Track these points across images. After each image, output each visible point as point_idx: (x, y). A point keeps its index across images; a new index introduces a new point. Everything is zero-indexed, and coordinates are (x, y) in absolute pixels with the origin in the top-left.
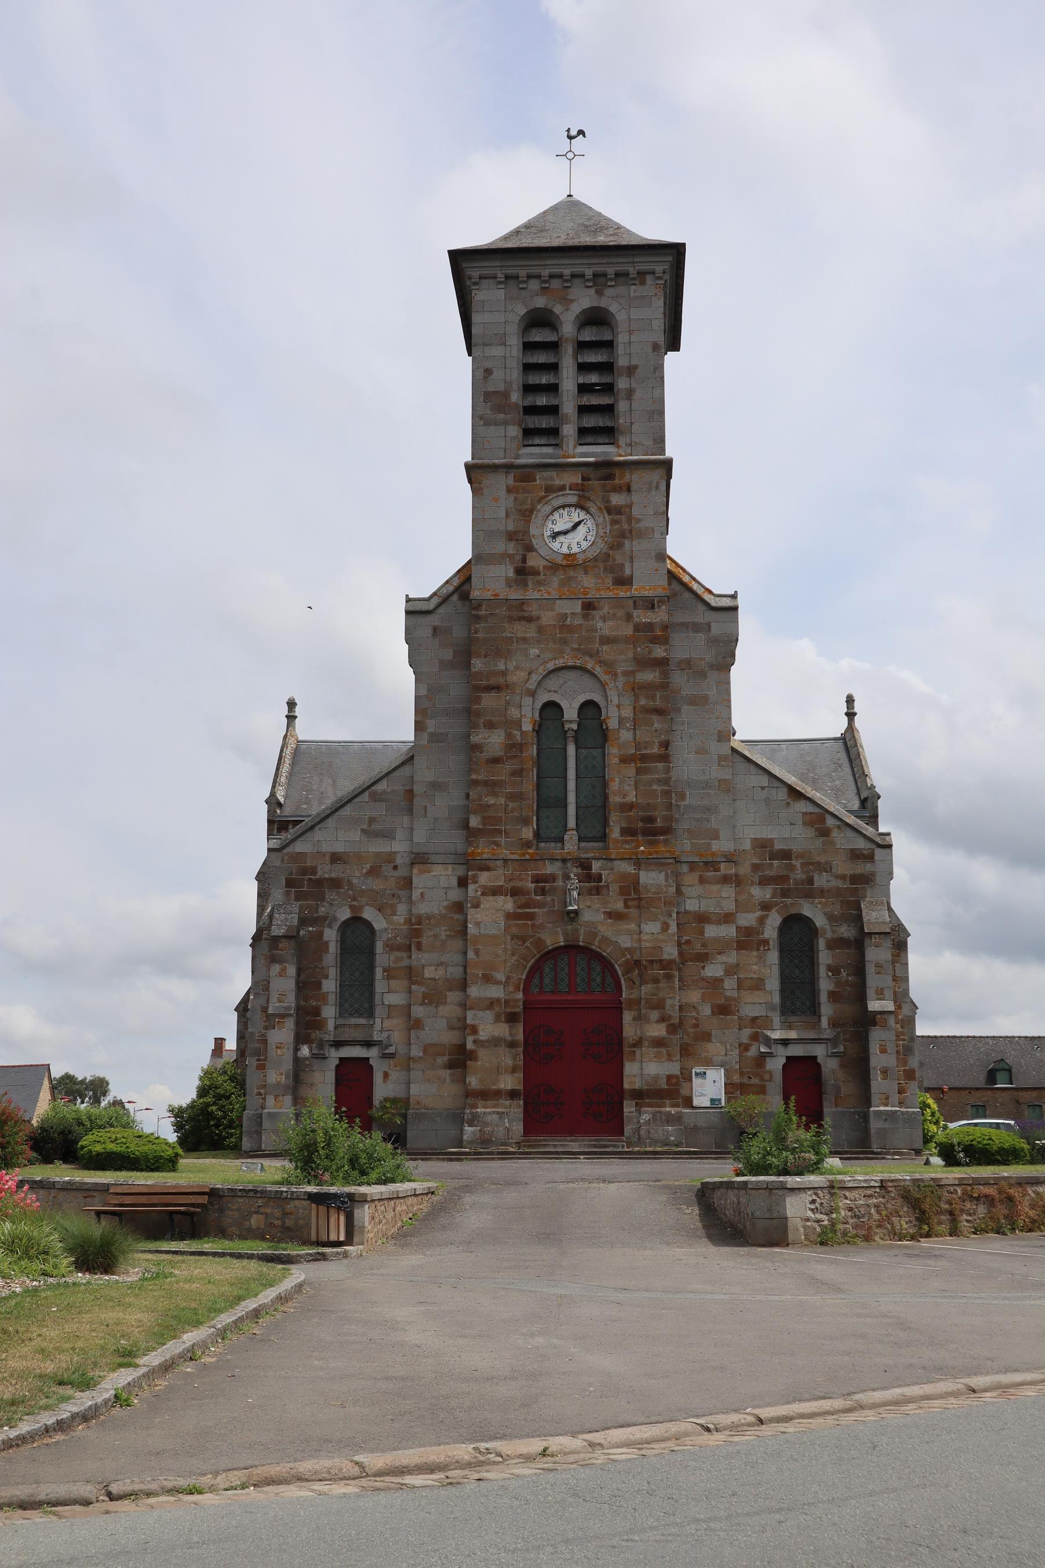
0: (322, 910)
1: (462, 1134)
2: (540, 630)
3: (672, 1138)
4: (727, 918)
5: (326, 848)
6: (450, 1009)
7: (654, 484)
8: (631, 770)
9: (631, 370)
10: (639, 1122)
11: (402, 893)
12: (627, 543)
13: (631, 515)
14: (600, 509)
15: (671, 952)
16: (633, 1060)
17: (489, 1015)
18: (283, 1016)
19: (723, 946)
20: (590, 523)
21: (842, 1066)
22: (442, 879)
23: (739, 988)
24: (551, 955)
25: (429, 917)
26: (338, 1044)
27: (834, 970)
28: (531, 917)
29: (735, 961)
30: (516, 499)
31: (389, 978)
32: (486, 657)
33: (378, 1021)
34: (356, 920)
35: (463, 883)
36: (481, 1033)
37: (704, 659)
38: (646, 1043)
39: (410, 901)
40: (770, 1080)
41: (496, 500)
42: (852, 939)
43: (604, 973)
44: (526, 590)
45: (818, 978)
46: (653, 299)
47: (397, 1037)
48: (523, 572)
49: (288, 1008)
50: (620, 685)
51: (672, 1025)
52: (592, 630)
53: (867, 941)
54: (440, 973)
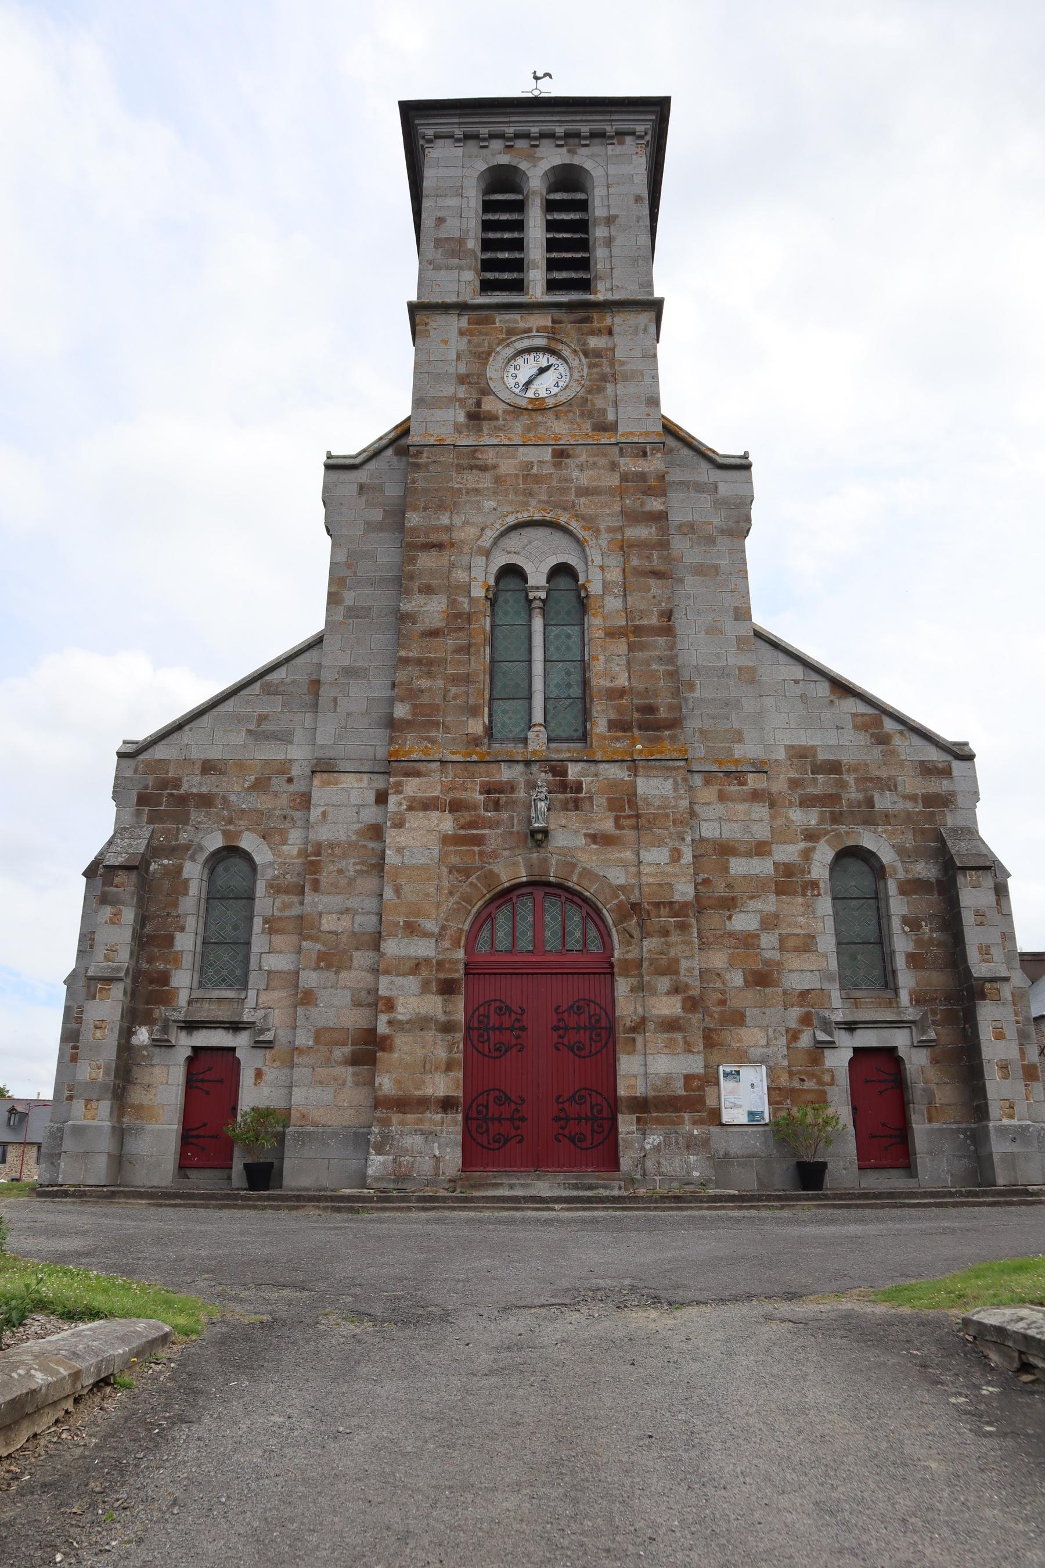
0: (184, 837)
1: (366, 1166)
2: (498, 480)
3: (696, 1174)
4: (761, 849)
5: (198, 754)
6: (356, 977)
7: (642, 326)
8: (620, 647)
9: (610, 220)
10: (643, 1148)
11: (298, 815)
12: (609, 387)
13: (613, 358)
14: (575, 351)
15: (684, 891)
16: (633, 1051)
17: (412, 983)
18: (109, 980)
19: (758, 887)
20: (562, 368)
21: (935, 1061)
22: (354, 794)
23: (782, 949)
24: (505, 895)
25: (332, 845)
26: (191, 1026)
27: (912, 924)
28: (479, 840)
29: (773, 909)
30: (469, 341)
31: (272, 931)
32: (425, 509)
33: (252, 994)
34: (232, 851)
35: (381, 798)
36: (400, 1009)
37: (711, 523)
38: (651, 1026)
39: (307, 825)
40: (832, 1084)
41: (445, 342)
42: (933, 880)
43: (584, 924)
44: (480, 436)
45: (890, 936)
46: (634, 157)
47: (277, 1018)
48: (476, 417)
49: (118, 969)
50: (604, 544)
51: (692, 998)
52: (566, 480)
53: (960, 880)
54: (344, 924)
